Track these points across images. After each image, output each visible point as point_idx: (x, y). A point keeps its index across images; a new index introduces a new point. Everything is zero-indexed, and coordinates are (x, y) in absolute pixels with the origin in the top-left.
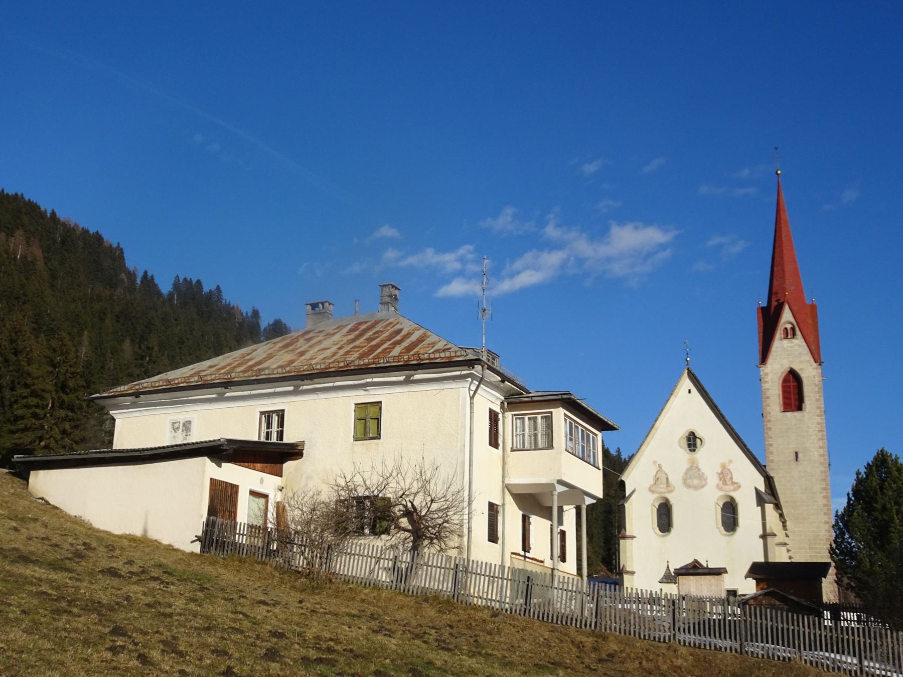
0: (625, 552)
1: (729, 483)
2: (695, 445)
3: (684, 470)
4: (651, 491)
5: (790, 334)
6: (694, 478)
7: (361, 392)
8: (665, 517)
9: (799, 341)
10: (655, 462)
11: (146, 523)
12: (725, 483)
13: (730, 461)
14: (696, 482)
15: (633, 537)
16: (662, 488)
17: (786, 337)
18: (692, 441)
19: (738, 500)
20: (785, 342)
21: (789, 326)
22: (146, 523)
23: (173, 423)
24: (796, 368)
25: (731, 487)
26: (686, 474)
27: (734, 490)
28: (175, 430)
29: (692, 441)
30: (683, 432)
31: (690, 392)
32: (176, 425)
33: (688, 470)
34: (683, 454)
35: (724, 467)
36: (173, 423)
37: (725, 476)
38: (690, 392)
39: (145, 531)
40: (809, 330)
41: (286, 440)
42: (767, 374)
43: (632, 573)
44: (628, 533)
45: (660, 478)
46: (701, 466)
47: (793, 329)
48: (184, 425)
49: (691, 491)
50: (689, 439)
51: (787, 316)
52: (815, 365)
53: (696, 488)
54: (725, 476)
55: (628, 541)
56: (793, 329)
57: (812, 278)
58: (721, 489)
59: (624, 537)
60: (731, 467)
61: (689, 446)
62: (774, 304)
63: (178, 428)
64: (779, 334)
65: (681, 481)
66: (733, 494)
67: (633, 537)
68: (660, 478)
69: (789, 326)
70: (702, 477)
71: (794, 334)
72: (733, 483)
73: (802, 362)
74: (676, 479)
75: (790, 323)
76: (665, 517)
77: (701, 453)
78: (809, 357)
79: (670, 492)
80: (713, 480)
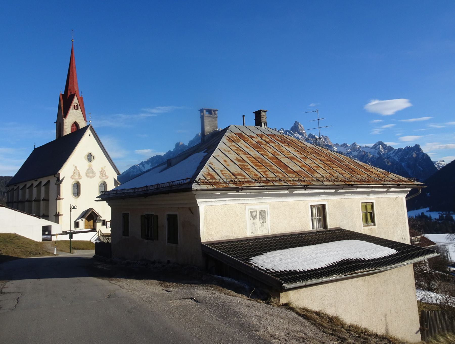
0: (60, 206)
1: (104, 176)
2: (91, 159)
3: (86, 170)
4: (71, 178)
5: (76, 108)
6: (90, 173)
7: (365, 196)
8: (77, 189)
9: (79, 111)
10: (74, 165)
11: (387, 325)
12: (103, 176)
13: (105, 167)
14: (91, 175)
15: (63, 199)
16: (76, 177)
17: (74, 109)
18: (90, 157)
19: (107, 183)
20: (74, 110)
21: (76, 105)
22: (387, 325)
23: (252, 212)
24: (78, 122)
25: (105, 178)
26: (87, 171)
27: (106, 179)
28: (254, 217)
29: (90, 157)
30: (86, 153)
31: (90, 135)
32: (254, 214)
33: (88, 170)
34: (86, 162)
35: (102, 169)
36: (252, 212)
37: (103, 173)
38: (90, 135)
39: (387, 332)
40: (81, 106)
41: (330, 226)
42: (66, 123)
43: (62, 215)
44: (61, 197)
45: (76, 172)
46: (93, 168)
47: (77, 106)
48: (260, 213)
49: (89, 179)
50: (88, 156)
51: (75, 101)
52: (85, 122)
53: (91, 177)
54: (103, 173)
55: (61, 201)
56: (77, 106)
57: (81, 86)
58: (101, 178)
59: (60, 199)
60: (105, 169)
61: (88, 159)
62: (69, 94)
63: (256, 216)
64: (72, 107)
65: (85, 174)
66: (105, 180)
67: (63, 199)
68: (76, 172)
69: (76, 105)
70: (93, 173)
71: (77, 108)
72: (106, 176)
73: (80, 120)
74: (83, 174)
75: (77, 103)
76: (77, 189)
77: (94, 163)
78: (83, 118)
79: (80, 179)
80: (98, 174)
